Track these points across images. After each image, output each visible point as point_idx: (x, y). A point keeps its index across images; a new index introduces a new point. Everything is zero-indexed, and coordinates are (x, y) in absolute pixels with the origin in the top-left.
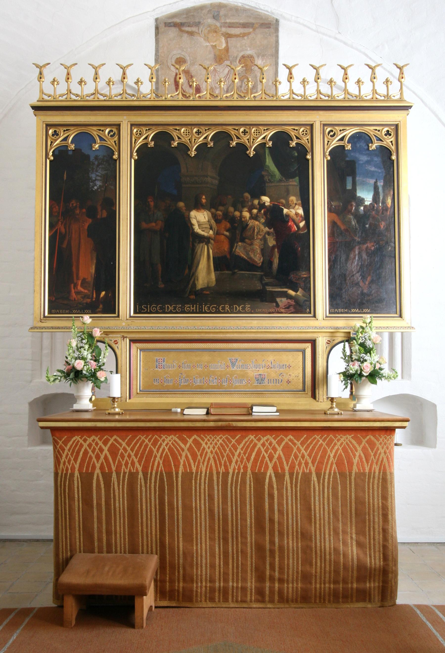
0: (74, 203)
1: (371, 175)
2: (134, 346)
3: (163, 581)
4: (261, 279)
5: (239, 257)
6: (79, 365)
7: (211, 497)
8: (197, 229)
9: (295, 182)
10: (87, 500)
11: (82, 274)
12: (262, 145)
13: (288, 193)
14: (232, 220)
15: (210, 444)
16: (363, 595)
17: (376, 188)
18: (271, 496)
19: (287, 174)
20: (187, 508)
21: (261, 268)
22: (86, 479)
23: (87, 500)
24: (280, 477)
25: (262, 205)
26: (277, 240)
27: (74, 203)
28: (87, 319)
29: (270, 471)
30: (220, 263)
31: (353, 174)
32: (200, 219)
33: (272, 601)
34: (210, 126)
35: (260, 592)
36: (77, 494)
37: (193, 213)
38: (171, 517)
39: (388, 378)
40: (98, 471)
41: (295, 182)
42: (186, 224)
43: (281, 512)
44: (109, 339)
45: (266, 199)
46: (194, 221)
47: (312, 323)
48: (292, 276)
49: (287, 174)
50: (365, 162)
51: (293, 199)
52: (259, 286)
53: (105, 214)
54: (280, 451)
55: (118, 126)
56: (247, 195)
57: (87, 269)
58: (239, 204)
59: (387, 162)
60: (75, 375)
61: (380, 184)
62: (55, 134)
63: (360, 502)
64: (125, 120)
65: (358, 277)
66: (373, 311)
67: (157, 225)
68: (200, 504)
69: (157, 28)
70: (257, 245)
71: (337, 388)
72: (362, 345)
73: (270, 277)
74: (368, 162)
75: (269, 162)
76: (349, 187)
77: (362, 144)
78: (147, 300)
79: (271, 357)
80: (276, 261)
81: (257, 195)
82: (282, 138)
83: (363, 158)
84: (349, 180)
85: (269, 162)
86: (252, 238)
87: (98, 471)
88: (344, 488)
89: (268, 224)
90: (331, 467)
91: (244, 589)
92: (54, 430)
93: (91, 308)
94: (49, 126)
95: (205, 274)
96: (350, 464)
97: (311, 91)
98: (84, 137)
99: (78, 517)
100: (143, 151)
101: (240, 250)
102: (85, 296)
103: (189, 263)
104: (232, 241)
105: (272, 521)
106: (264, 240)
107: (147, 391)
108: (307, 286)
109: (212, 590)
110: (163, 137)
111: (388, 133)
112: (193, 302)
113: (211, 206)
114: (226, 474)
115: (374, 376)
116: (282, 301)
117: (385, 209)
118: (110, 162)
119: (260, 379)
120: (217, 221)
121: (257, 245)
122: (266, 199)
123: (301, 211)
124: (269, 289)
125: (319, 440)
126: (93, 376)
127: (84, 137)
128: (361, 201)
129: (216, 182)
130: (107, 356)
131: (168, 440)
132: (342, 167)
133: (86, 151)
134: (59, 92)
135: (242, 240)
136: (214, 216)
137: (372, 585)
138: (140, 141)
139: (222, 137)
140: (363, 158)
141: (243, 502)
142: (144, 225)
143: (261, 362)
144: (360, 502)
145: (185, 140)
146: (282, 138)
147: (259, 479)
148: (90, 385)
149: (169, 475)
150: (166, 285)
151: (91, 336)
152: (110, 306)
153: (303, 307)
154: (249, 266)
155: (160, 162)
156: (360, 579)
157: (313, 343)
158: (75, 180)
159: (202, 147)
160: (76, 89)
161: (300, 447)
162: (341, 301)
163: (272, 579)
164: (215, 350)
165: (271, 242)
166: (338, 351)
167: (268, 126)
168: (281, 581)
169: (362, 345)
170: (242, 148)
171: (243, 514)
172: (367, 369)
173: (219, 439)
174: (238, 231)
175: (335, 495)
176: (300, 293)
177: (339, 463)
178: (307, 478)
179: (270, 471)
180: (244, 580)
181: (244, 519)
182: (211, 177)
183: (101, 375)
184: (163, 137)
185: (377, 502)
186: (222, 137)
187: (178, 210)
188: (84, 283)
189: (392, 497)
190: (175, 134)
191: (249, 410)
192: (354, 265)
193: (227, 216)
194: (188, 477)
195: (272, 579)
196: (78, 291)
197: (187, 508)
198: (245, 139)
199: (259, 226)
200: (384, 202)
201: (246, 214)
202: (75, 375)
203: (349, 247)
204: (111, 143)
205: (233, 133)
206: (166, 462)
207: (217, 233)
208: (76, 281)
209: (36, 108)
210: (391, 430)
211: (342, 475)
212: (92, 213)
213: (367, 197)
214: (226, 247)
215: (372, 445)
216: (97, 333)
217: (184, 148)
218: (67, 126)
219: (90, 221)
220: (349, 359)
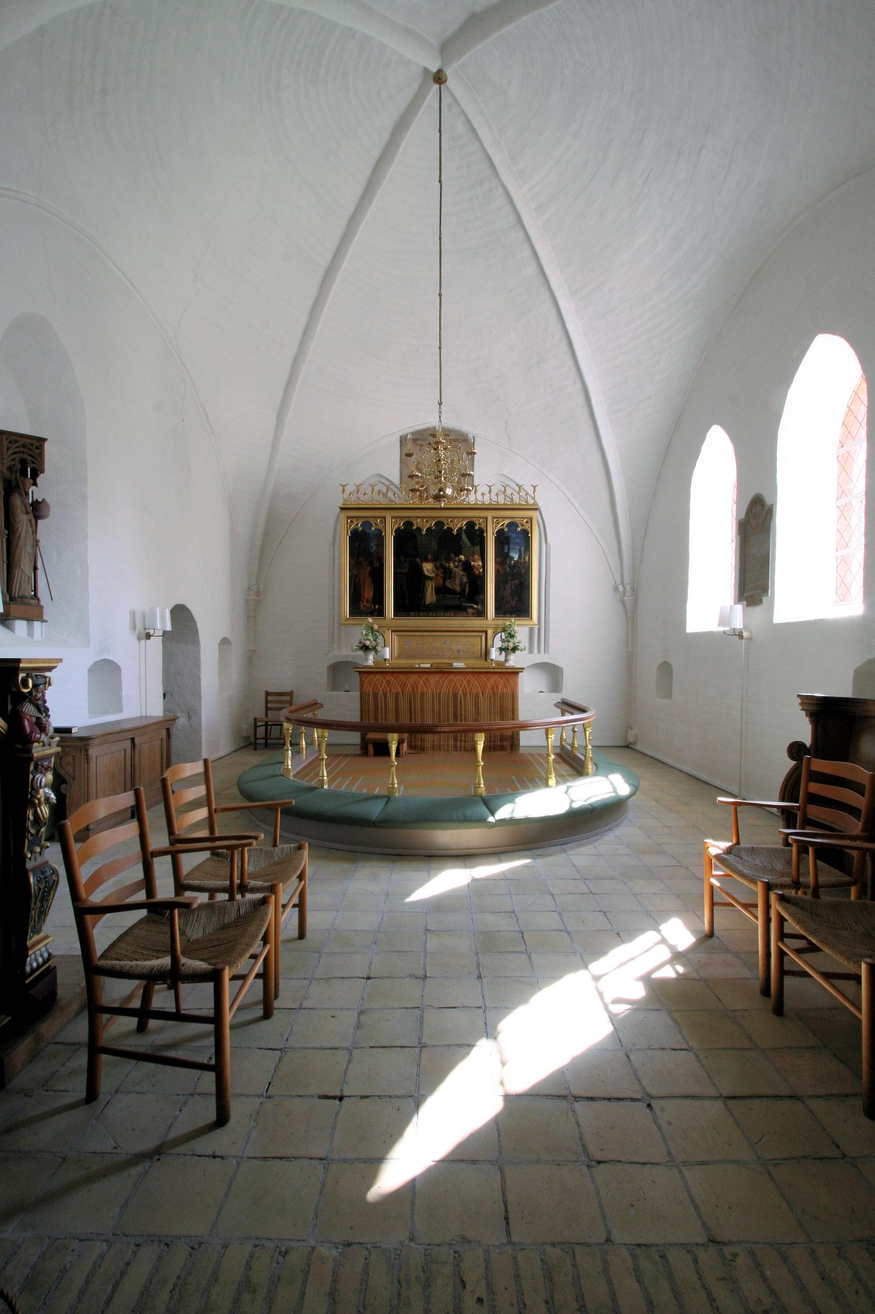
0: (361, 559)
1: (518, 544)
2: (394, 634)
3: (411, 742)
4: (459, 599)
5: (448, 588)
6: (367, 643)
7: (433, 704)
8: (426, 573)
9: (477, 548)
10: (376, 706)
11: (366, 596)
12: (461, 528)
13: (474, 554)
14: (445, 568)
15: (433, 679)
16: (502, 748)
17: (520, 551)
18: (461, 703)
19: (473, 544)
20: (422, 709)
21: (460, 593)
22: (376, 695)
23: (376, 706)
24: (465, 694)
25: (460, 560)
26: (468, 578)
27: (361, 559)
28: (370, 620)
29: (460, 692)
30: (438, 591)
31: (508, 543)
32: (428, 568)
33: (461, 750)
34: (433, 518)
35: (455, 747)
36: (371, 702)
37: (424, 564)
38: (415, 712)
39: (521, 650)
40: (381, 692)
41: (477, 548)
42: (420, 570)
43: (465, 710)
44: (381, 630)
45: (462, 557)
46: (424, 569)
47: (485, 622)
48: (476, 598)
49: (473, 544)
50: (516, 538)
51: (476, 557)
52: (458, 603)
53: (378, 564)
54: (465, 682)
55: (385, 518)
56: (452, 555)
57: (368, 593)
58: (448, 560)
59: (526, 537)
60: (365, 648)
61: (523, 549)
62: (351, 522)
63: (502, 706)
64: (388, 515)
65: (510, 598)
66: (518, 616)
67: (405, 571)
68: (428, 707)
69: (401, 442)
70: (457, 581)
71: (494, 654)
72: (509, 634)
73: (465, 598)
74: (516, 538)
75: (464, 537)
76: (506, 550)
77: (513, 528)
78: (401, 609)
79: (464, 640)
80: (467, 590)
81: (457, 555)
82: (471, 525)
83: (514, 535)
84: (506, 547)
85: (464, 537)
86: (455, 578)
87: (381, 692)
88: (494, 700)
89: (464, 570)
90: (489, 691)
91: (448, 745)
92: (360, 673)
93: (371, 614)
94: (348, 518)
95: (430, 597)
96: (498, 689)
97: (487, 500)
98: (367, 524)
99: (372, 713)
100: (398, 531)
101: (448, 584)
102: (368, 608)
103: (422, 591)
104: (444, 579)
105: (461, 714)
106: (462, 579)
107: (400, 657)
108: (483, 603)
109: (434, 746)
110: (408, 524)
111: (527, 522)
112: (424, 611)
113: (434, 560)
114: (440, 693)
115: (515, 649)
116: (470, 611)
117: (525, 562)
118: (380, 538)
119: (458, 651)
120: (437, 568)
121: (457, 581)
122: (462, 557)
123: (480, 564)
124: (464, 604)
125: (483, 677)
126: (375, 649)
127: (367, 524)
128: (512, 558)
129: (436, 548)
130: (380, 640)
131: (413, 678)
132: (502, 539)
133: (367, 530)
134: (353, 501)
135: (450, 578)
136: (435, 566)
137: (507, 744)
138: (396, 526)
139: (439, 524)
140: (514, 535)
141: (448, 705)
142: (398, 571)
143: (451, 641)
144: (502, 706)
145: (420, 525)
146: (471, 525)
147: (455, 695)
148: (373, 652)
149: (414, 693)
150: (410, 603)
151: (372, 628)
152: (381, 613)
153: (481, 613)
154: (453, 592)
155: (406, 538)
156: (501, 741)
157: (486, 632)
158: (363, 547)
159: (429, 530)
160: (362, 498)
161: (474, 681)
162: (501, 610)
163: (461, 741)
164: (423, 636)
165: (465, 580)
166: (498, 637)
167: (464, 518)
168: (465, 741)
169: (509, 634)
170: (450, 530)
171: (448, 711)
172: (511, 645)
173: (437, 677)
174: (448, 574)
175: (490, 703)
176: (479, 607)
177: (492, 689)
178: (477, 695)
179: (460, 692)
180: (448, 741)
181: (448, 714)
182: (434, 546)
183: (379, 648)
184: (408, 524)
185: (510, 706)
186: (439, 524)
187: (416, 563)
188: (367, 601)
189: (517, 704)
190: (414, 522)
191: (451, 664)
192: (507, 593)
193: (441, 565)
194: (502, 694)
195: (461, 741)
196: (364, 605)
197: (422, 709)
198: (451, 525)
199: (459, 572)
200: (524, 559)
201: (452, 565)
202: (365, 648)
203: (505, 582)
204: (381, 527)
205: (445, 521)
206: (412, 687)
207: (437, 575)
208: (365, 601)
209: (342, 509)
210: (517, 673)
211: (494, 694)
212: (371, 564)
213: (516, 557)
214: (441, 582)
215: (508, 680)
216: (376, 627)
217: (419, 530)
218: (358, 518)
219: (370, 568)
220: (503, 641)
